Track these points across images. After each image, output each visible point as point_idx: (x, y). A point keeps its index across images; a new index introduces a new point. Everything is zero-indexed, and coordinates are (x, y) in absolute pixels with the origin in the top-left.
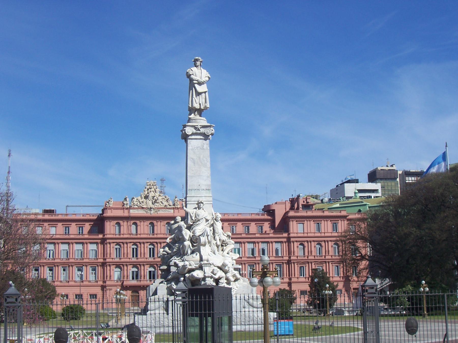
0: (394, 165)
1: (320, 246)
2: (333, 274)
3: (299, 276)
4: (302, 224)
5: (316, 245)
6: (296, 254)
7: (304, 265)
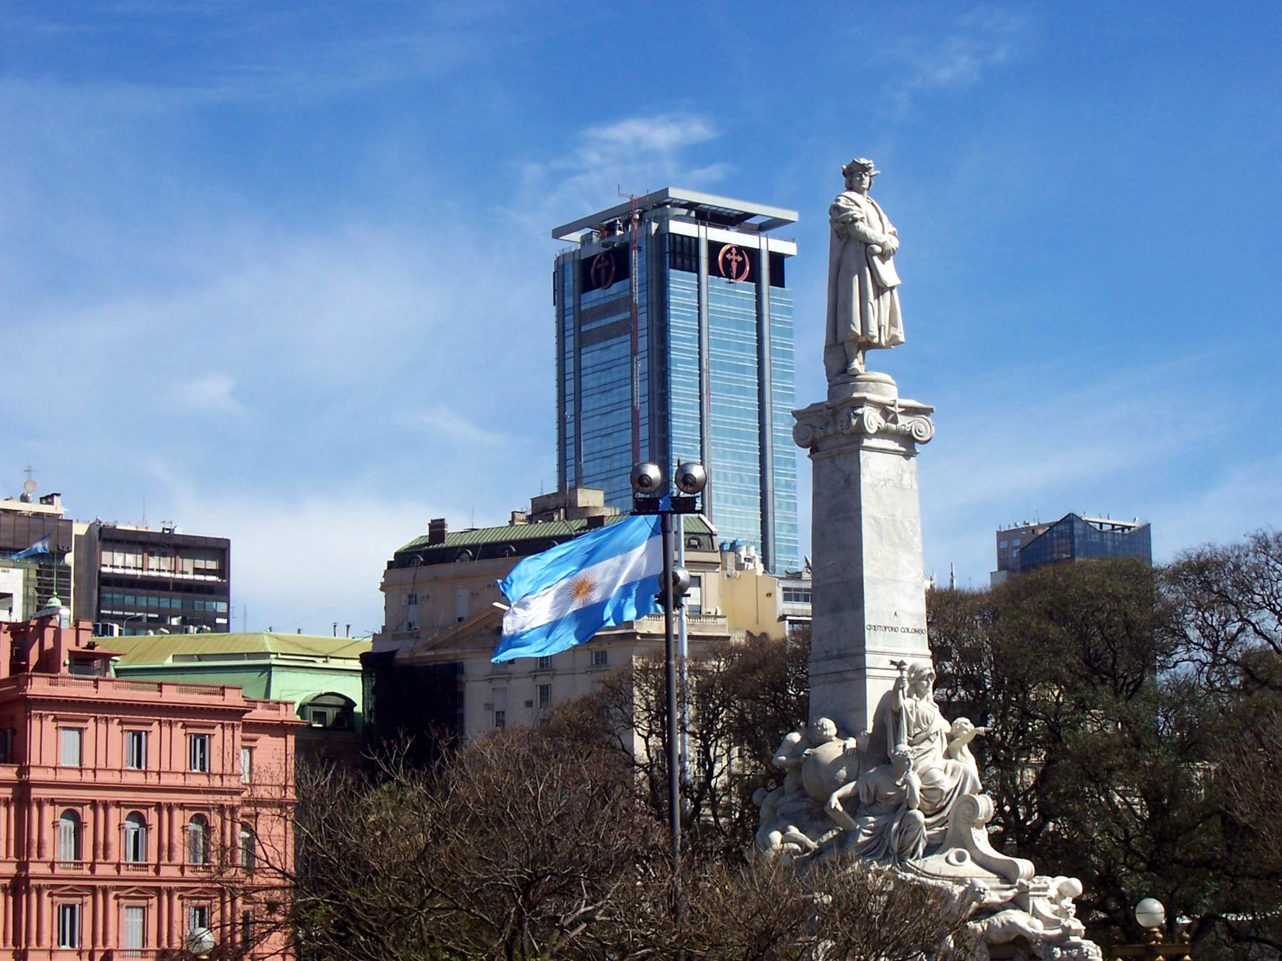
0: (55, 497)
1: (137, 826)
2: (52, 939)
3: (55, 942)
4: (76, 733)
5: (123, 821)
6: (48, 855)
7: (77, 900)
